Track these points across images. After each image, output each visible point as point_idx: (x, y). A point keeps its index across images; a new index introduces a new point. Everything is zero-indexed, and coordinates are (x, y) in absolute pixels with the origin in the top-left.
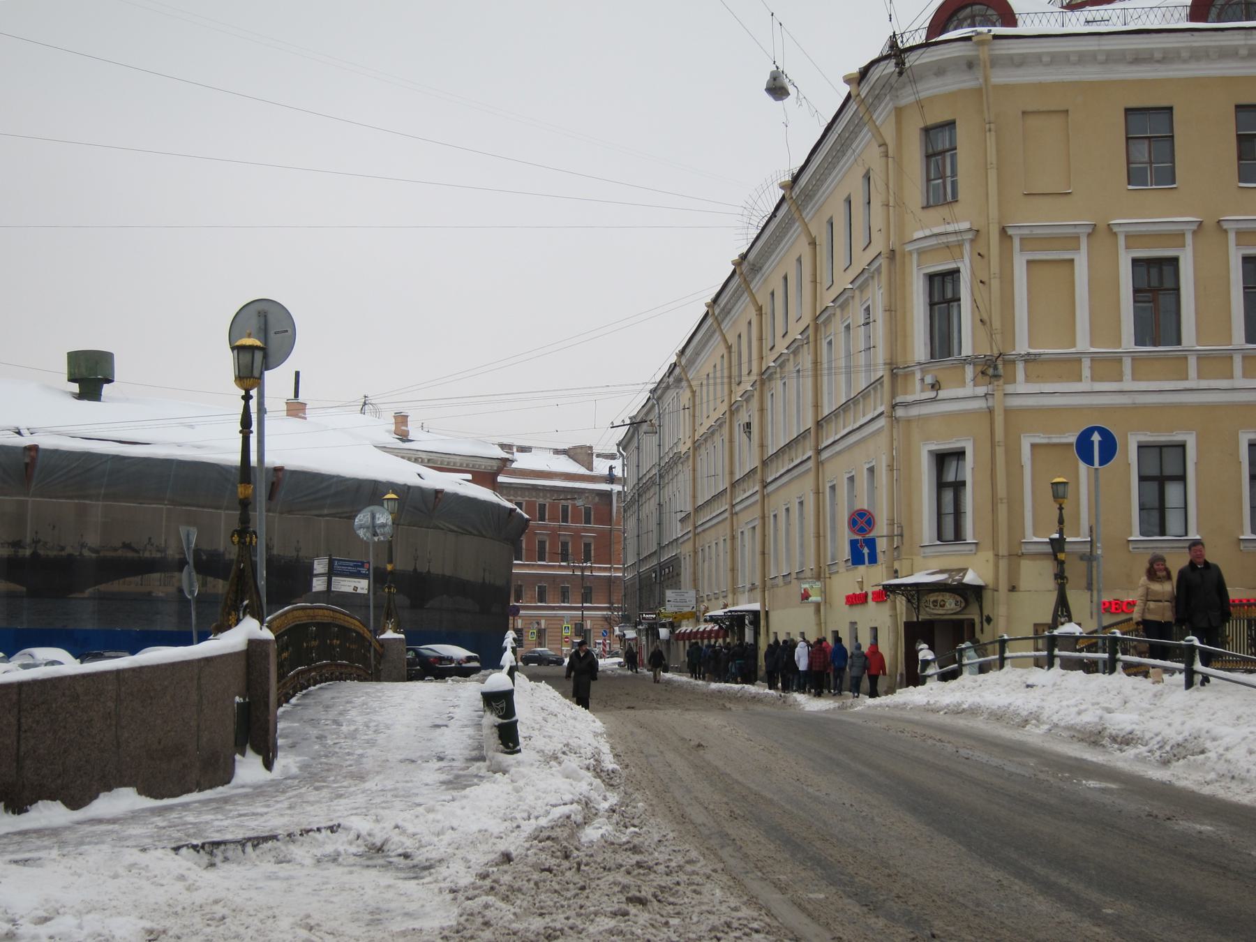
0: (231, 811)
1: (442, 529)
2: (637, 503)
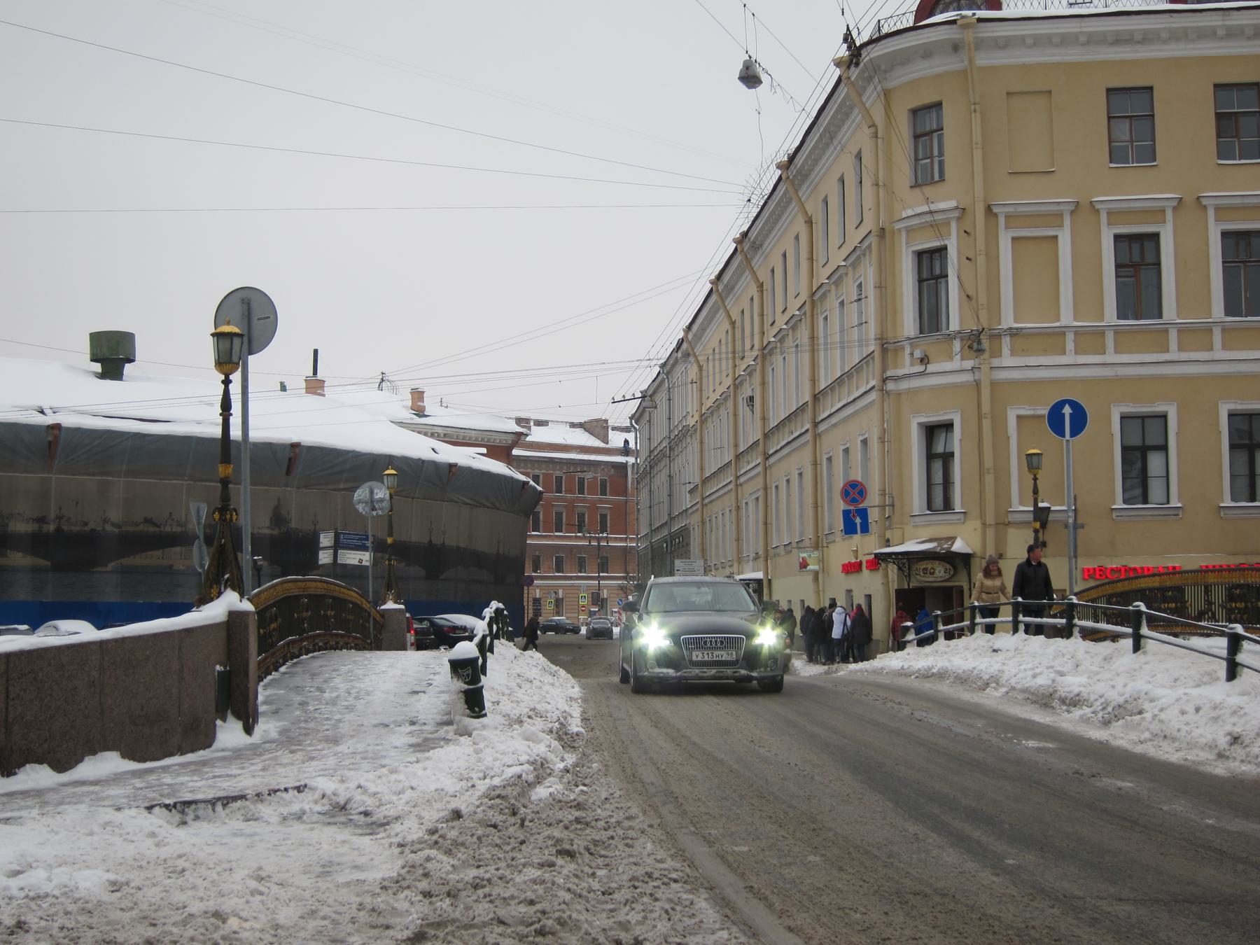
0: (207, 773)
1: (457, 502)
2: (648, 475)
